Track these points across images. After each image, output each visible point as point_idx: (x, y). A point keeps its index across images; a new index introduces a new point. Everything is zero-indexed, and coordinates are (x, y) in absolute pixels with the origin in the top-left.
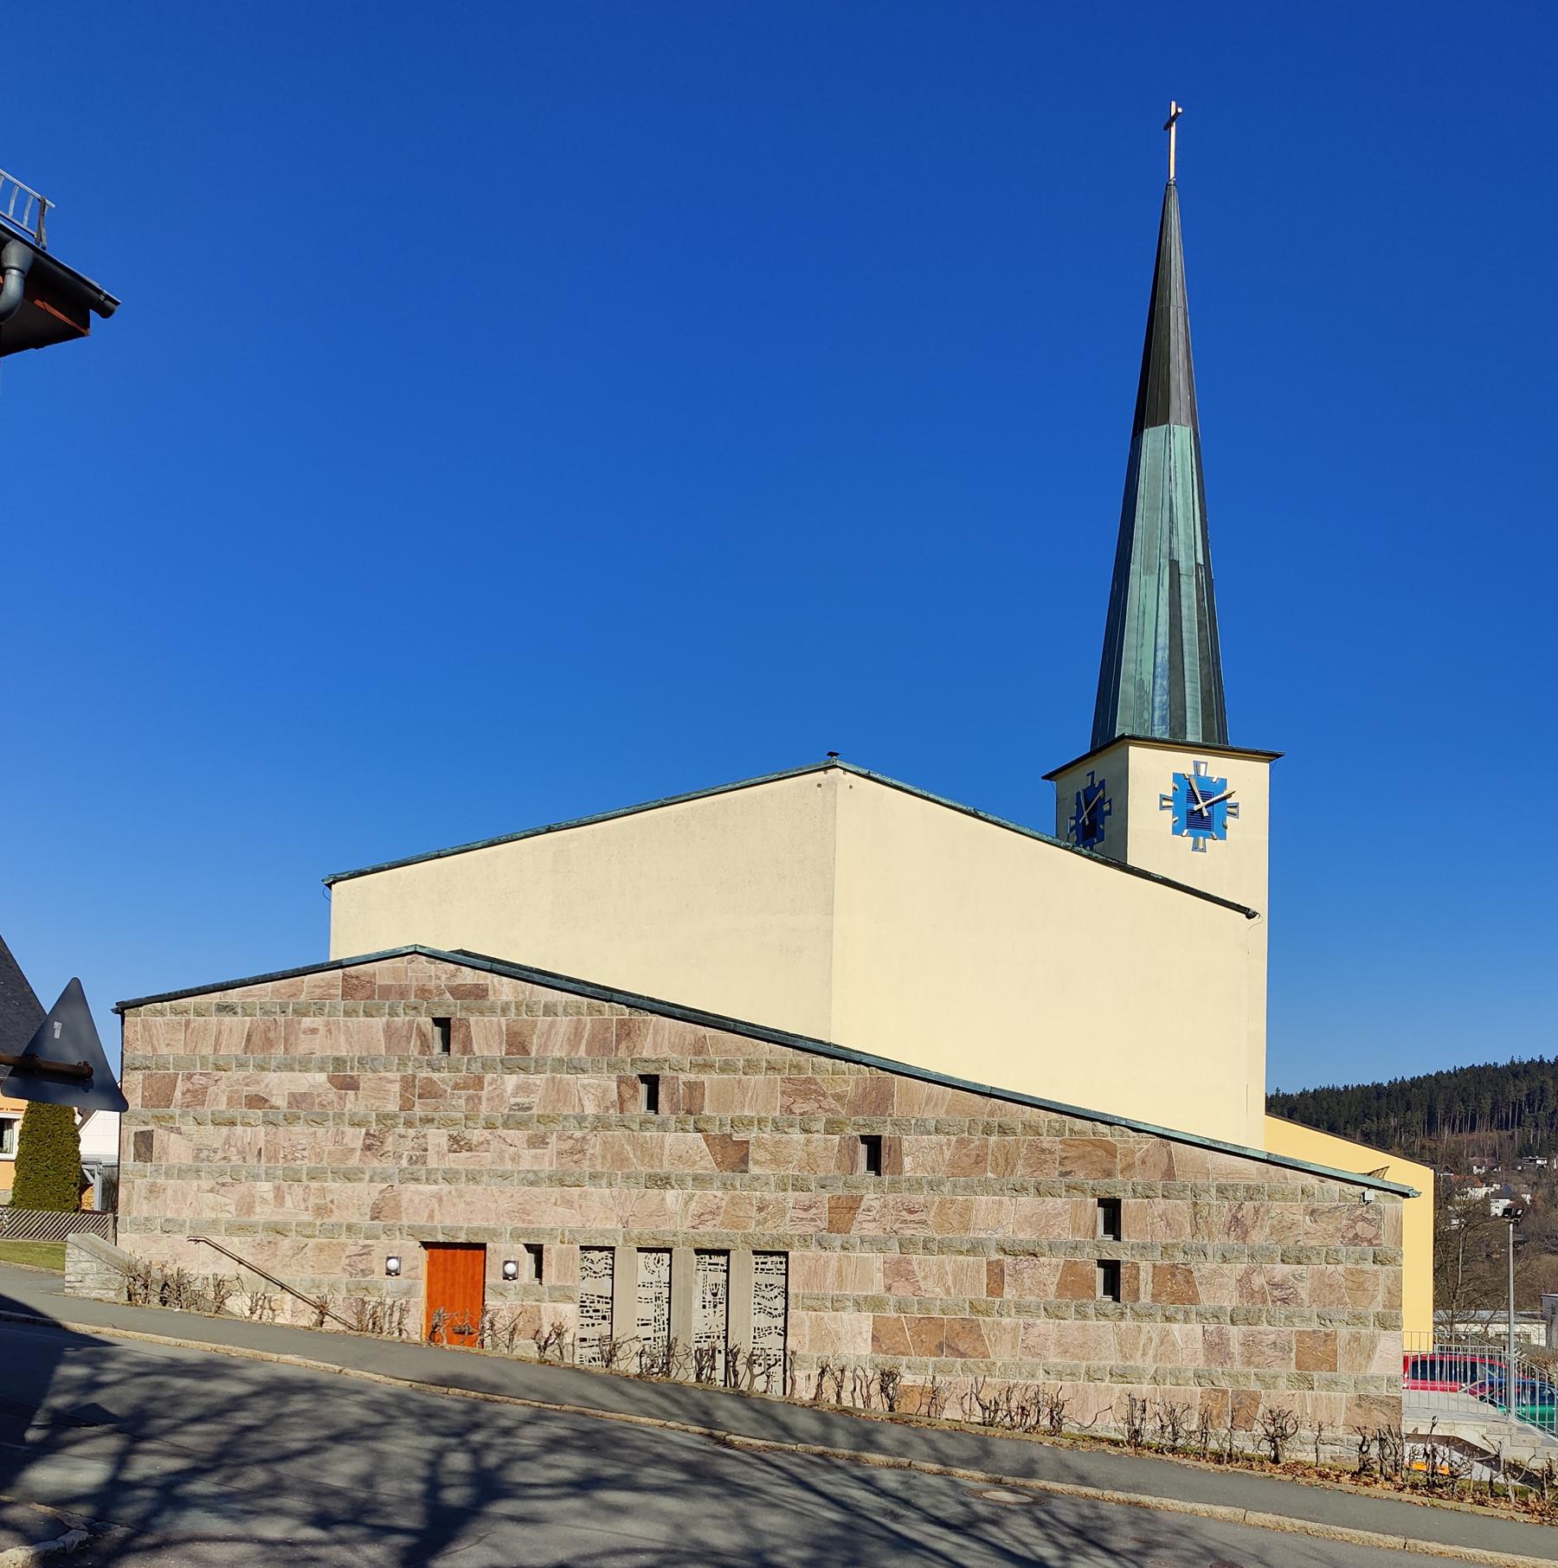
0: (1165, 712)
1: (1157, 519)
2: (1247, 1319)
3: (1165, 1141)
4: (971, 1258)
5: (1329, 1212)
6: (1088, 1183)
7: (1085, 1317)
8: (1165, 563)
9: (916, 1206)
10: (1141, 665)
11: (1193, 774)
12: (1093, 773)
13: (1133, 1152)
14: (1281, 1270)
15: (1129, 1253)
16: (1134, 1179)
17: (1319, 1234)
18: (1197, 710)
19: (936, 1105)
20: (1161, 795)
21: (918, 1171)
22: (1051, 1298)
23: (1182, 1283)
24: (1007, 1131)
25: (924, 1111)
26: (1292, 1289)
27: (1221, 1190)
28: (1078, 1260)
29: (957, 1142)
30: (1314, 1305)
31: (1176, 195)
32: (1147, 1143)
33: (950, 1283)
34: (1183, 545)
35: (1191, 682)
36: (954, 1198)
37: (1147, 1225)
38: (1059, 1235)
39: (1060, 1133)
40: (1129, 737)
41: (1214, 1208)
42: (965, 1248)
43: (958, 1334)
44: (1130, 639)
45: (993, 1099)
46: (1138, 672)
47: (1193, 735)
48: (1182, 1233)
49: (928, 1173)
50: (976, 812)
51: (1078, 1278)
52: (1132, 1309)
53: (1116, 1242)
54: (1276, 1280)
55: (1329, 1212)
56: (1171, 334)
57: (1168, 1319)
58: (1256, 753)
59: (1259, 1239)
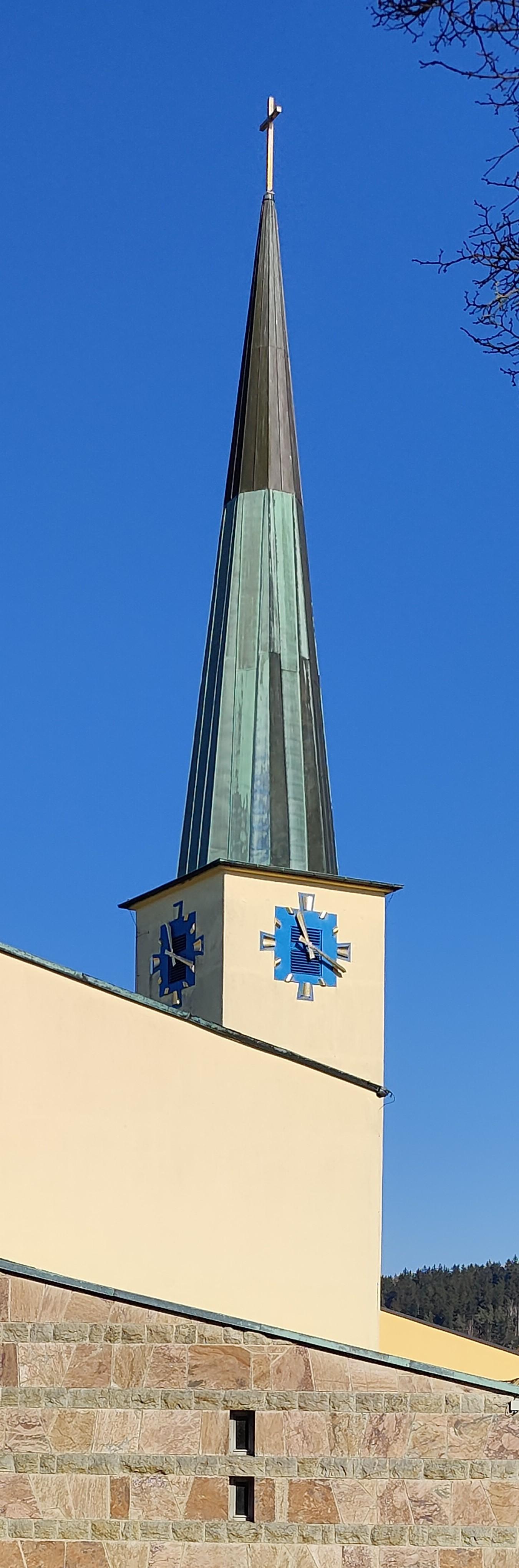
0: (265, 834)
1: (255, 603)
2: (389, 1538)
3: (302, 1348)
4: (94, 1477)
5: (474, 1423)
6: (219, 1394)
7: (217, 1538)
8: (265, 655)
9: (34, 1420)
10: (236, 776)
11: (298, 908)
12: (181, 903)
13: (268, 1360)
14: (424, 1486)
15: (263, 1469)
16: (269, 1389)
17: (464, 1446)
18: (302, 832)
19: (54, 1309)
20: (261, 933)
21: (35, 1381)
22: (180, 1518)
23: (320, 1500)
24: (132, 1338)
25: (41, 1316)
26: (436, 1506)
27: (361, 1401)
28: (209, 1477)
29: (77, 1349)
30: (459, 1523)
31: (275, 211)
32: (282, 1350)
33: (71, 1504)
34: (285, 636)
35: (295, 798)
36: (75, 1410)
37: (282, 1439)
38: (189, 1450)
39: (189, 1339)
40: (227, 864)
41: (354, 1419)
42: (86, 1466)
43: (79, 1559)
44: (223, 744)
45: (116, 1302)
46: (234, 784)
47: (298, 864)
48: (320, 1447)
49: (47, 1384)
50: (84, 977)
51: (209, 1497)
52: (266, 1528)
53: (250, 1458)
54: (419, 1496)
55: (474, 1423)
56: (270, 381)
57: (305, 1539)
58: (370, 885)
59: (401, 1453)
